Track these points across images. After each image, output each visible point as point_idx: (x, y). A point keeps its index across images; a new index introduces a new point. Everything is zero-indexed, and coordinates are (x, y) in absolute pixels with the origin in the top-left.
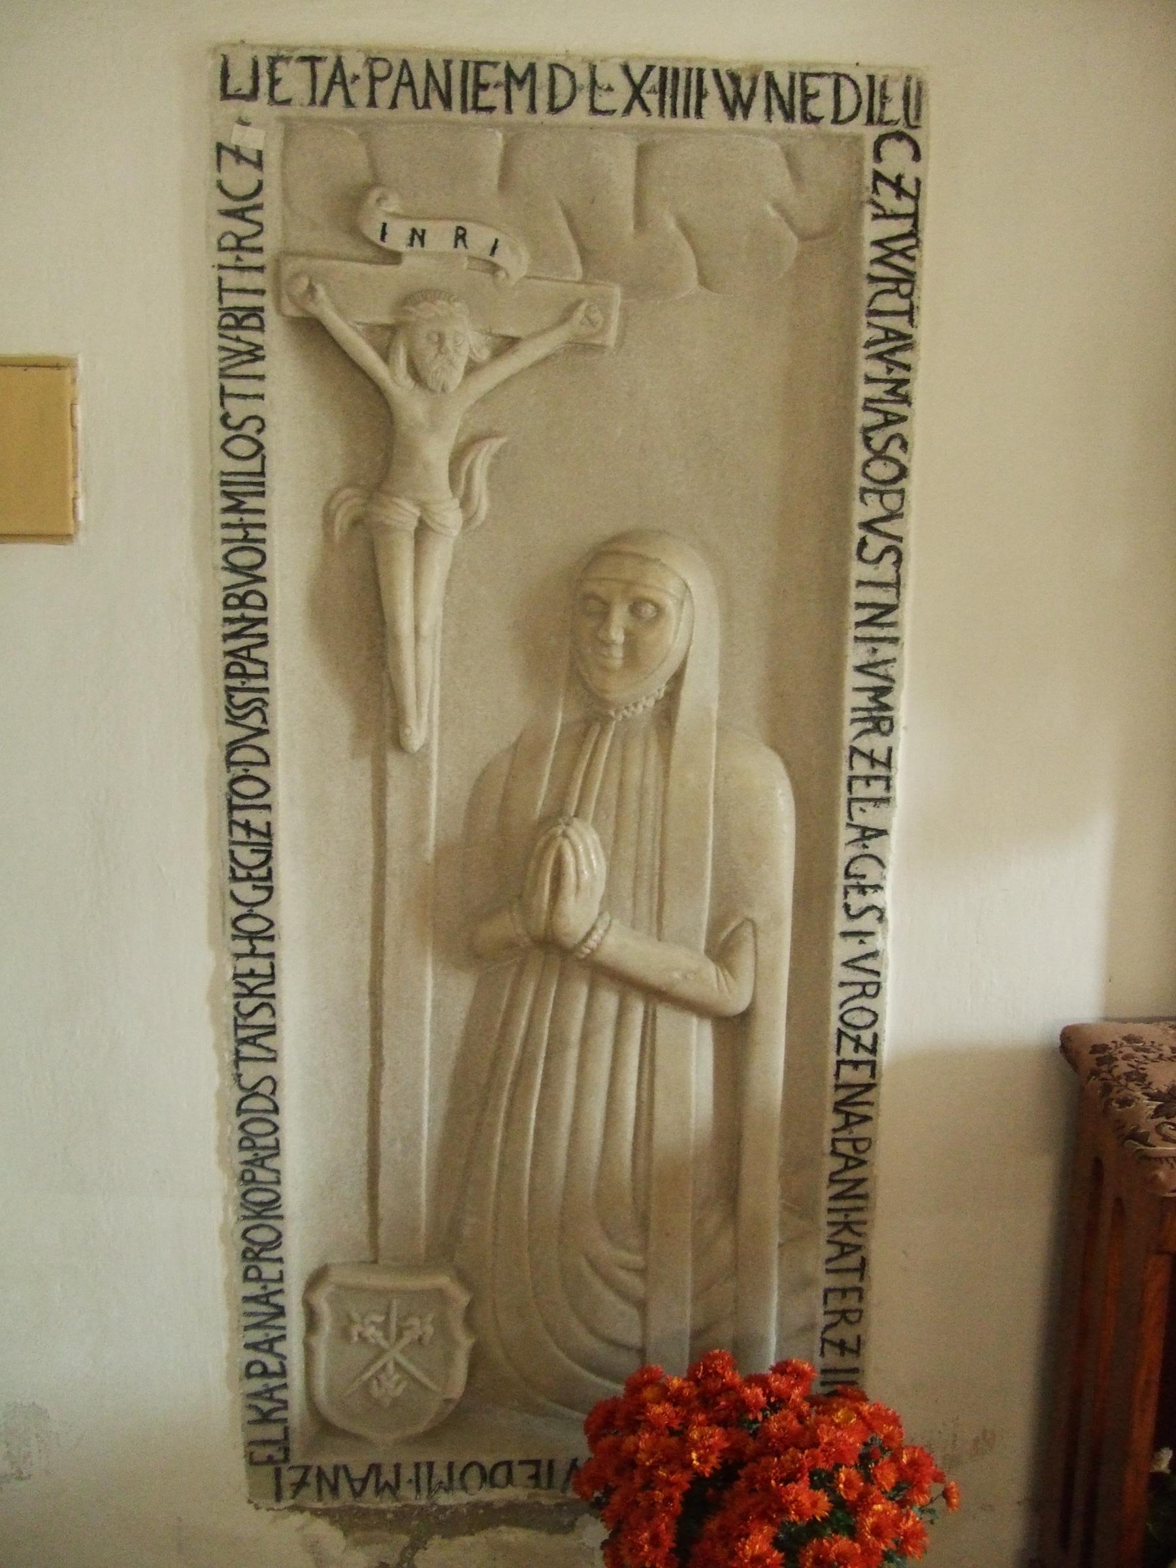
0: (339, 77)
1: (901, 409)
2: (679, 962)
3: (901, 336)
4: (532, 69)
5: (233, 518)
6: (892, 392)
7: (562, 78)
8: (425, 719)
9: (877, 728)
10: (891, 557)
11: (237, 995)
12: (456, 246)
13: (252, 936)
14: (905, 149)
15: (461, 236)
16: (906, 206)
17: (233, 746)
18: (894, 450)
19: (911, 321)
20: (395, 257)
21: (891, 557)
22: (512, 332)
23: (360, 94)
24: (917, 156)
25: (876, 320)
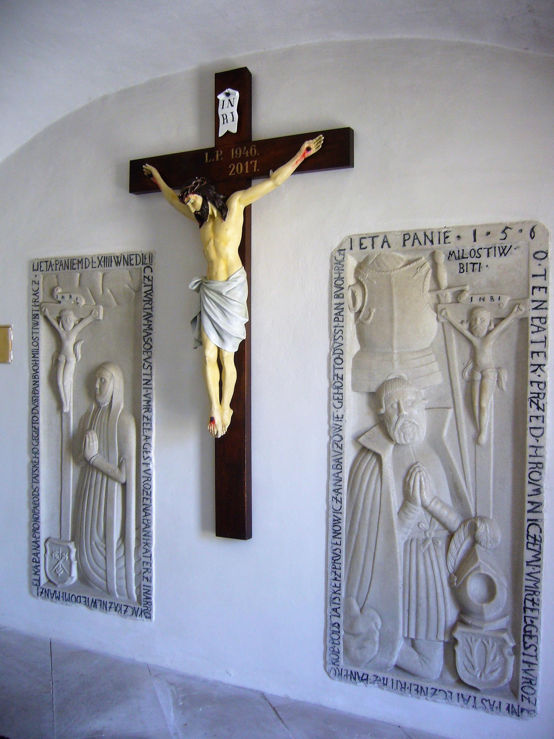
0: (51, 265)
1: (150, 331)
2: (111, 467)
3: (150, 314)
4: (82, 260)
5: (34, 359)
6: (535, 584)
7: (87, 260)
8: (68, 405)
9: (148, 411)
10: (149, 368)
12: (382, 247)
13: (338, 388)
14: (149, 269)
15: (70, 297)
16: (150, 283)
17: (33, 409)
18: (149, 341)
20: (60, 302)
21: (149, 368)
22: (82, 317)
23: (54, 267)
24: (152, 271)
25: (145, 311)
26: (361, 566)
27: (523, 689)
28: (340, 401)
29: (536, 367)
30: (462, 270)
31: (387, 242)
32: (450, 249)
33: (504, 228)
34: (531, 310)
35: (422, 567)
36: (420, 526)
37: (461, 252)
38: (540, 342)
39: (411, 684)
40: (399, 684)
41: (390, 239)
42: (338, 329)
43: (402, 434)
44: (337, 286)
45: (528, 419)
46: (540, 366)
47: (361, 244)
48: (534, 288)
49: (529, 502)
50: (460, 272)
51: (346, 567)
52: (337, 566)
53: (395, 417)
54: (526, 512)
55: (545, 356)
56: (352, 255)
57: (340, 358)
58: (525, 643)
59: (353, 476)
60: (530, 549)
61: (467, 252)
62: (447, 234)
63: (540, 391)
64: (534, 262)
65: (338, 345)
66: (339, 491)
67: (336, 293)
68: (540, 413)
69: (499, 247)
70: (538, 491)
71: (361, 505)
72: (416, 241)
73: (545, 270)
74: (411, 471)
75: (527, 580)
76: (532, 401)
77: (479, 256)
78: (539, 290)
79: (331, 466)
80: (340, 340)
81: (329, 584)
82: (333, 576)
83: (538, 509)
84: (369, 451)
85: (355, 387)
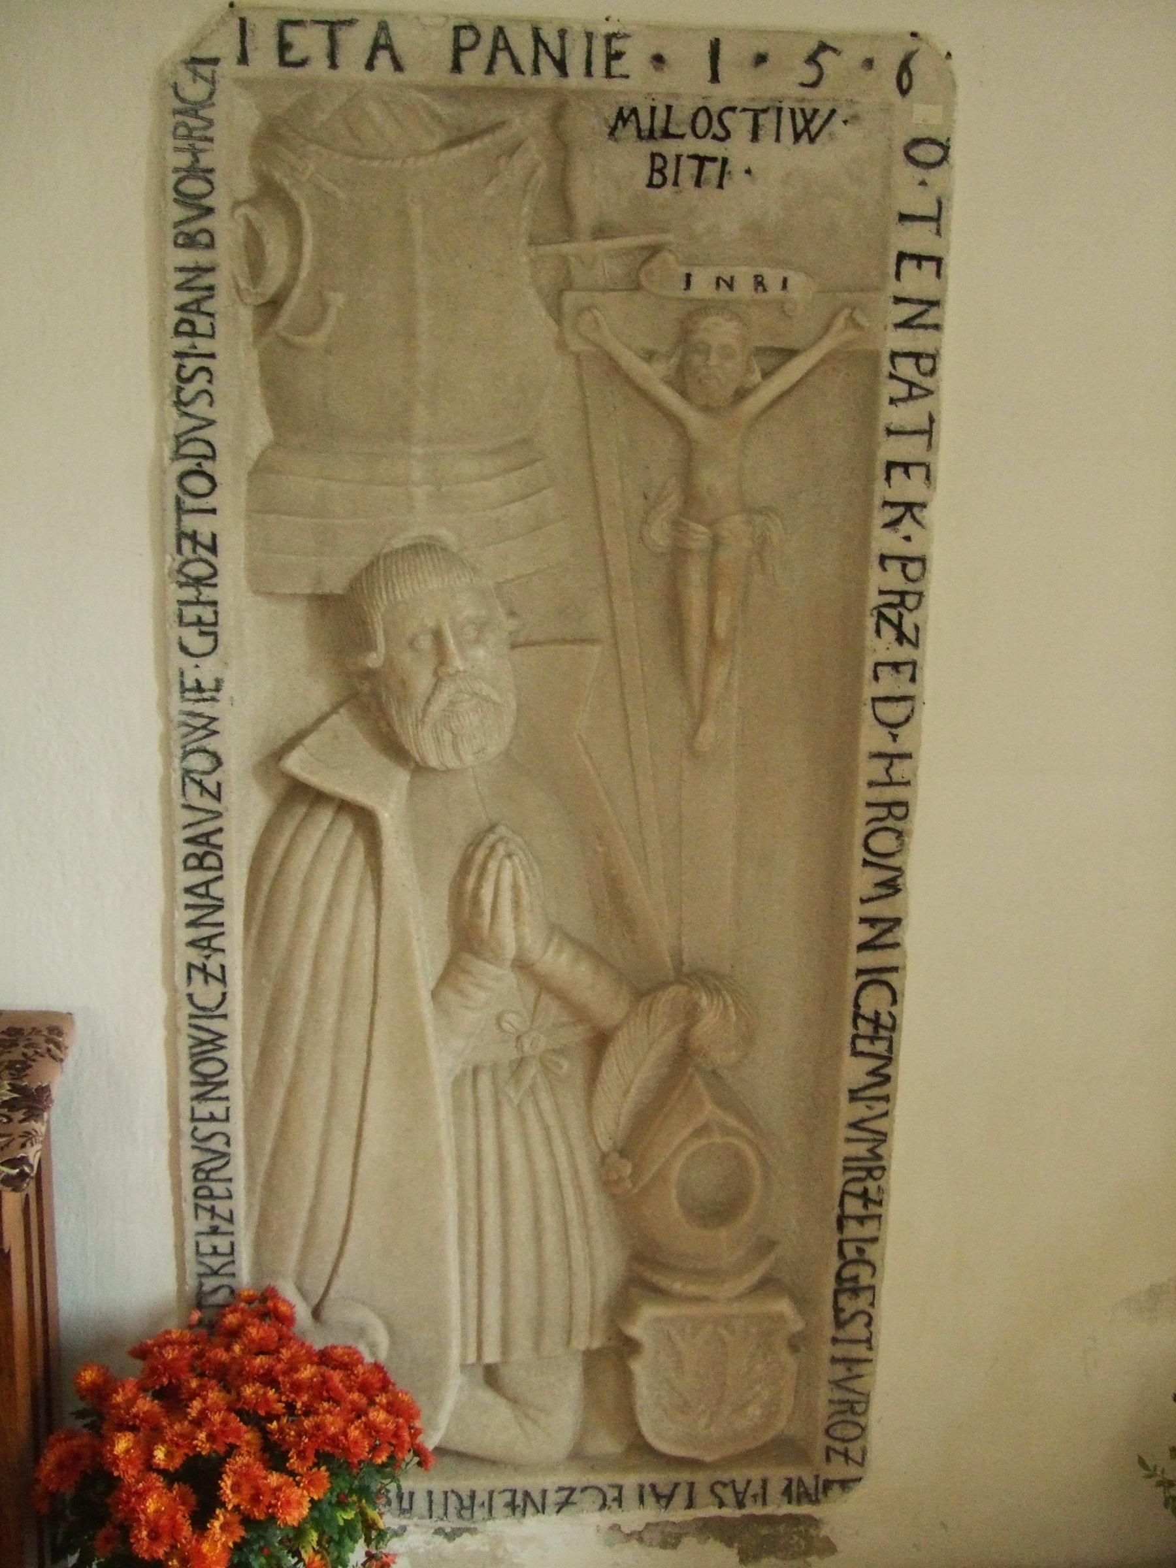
6: (871, 1150)
11: (200, 1275)
12: (370, 65)
13: (198, 581)
19: (870, 1348)
26: (310, 1178)
27: (831, 1432)
28: (208, 629)
29: (899, 511)
30: (659, 173)
31: (389, 47)
32: (622, 100)
33: (813, 45)
34: (891, 327)
35: (515, 1152)
36: (505, 1025)
37: (661, 114)
38: (915, 432)
39: (491, 1493)
40: (453, 1499)
41: (401, 37)
42: (191, 364)
43: (447, 737)
44: (189, 203)
45: (868, 673)
46: (909, 506)
47: (284, 46)
48: (901, 256)
49: (863, 920)
50: (650, 185)
51: (250, 1191)
52: (219, 1189)
53: (423, 682)
54: (854, 949)
55: (928, 477)
56: (246, 84)
57: (203, 473)
58: (837, 1310)
59: (265, 887)
60: (862, 1054)
61: (683, 113)
62: (617, 45)
63: (910, 587)
64: (906, 174)
65: (194, 423)
66: (215, 943)
67: (186, 228)
68: (902, 653)
69: (793, 111)
70: (892, 887)
71: (301, 981)
72: (503, 59)
73: (940, 203)
74: (480, 855)
75: (849, 1140)
76: (881, 615)
77: (721, 133)
78: (919, 266)
79: (179, 859)
80: (200, 407)
81: (190, 1252)
82: (205, 1221)
83: (888, 939)
84: (319, 797)
85: (261, 584)
